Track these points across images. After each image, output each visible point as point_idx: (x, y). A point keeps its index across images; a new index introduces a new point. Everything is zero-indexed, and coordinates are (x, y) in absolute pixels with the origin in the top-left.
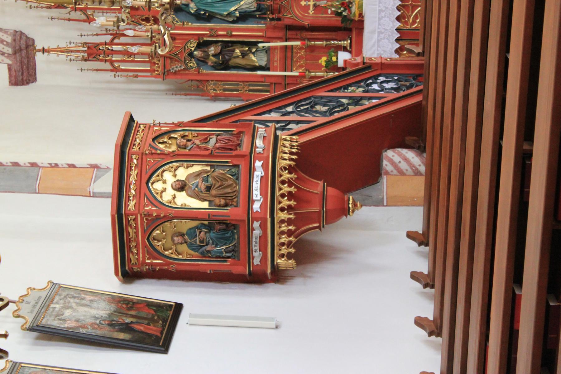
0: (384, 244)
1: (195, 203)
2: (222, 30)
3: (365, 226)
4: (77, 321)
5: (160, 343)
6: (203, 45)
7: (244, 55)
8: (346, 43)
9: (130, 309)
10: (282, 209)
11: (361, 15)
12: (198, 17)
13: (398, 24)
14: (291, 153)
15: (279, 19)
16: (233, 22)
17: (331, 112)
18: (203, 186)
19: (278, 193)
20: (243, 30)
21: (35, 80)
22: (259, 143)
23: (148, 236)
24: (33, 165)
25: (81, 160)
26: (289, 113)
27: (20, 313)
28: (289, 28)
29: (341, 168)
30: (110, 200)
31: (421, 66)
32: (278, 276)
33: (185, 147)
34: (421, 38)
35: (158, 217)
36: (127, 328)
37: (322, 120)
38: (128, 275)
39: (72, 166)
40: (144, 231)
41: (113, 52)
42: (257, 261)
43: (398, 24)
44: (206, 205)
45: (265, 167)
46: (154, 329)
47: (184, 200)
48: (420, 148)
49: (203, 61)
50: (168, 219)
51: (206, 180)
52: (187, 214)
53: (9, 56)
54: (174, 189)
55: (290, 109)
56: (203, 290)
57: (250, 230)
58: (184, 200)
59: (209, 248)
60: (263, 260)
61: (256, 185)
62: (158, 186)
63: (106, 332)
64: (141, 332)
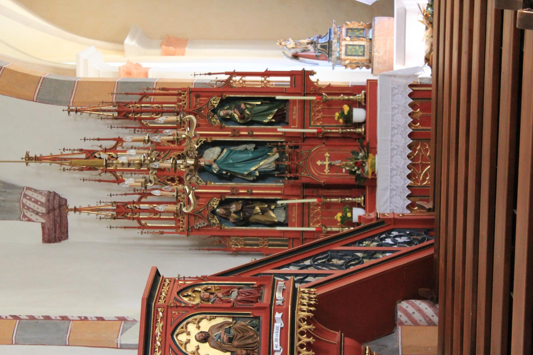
2: (243, 189)
6: (225, 203)
7: (264, 211)
8: (360, 200)
11: (374, 173)
12: (220, 177)
13: (409, 182)
14: (310, 305)
18: (225, 337)
19: (297, 344)
20: (262, 189)
21: (67, 237)
22: (279, 295)
26: (307, 267)
28: (306, 186)
31: (431, 221)
37: (338, 273)
39: (101, 319)
43: (409, 182)
45: (284, 318)
48: (433, 300)
49: (224, 218)
51: (228, 331)
55: (308, 263)
61: (276, 336)
62: (183, 338)
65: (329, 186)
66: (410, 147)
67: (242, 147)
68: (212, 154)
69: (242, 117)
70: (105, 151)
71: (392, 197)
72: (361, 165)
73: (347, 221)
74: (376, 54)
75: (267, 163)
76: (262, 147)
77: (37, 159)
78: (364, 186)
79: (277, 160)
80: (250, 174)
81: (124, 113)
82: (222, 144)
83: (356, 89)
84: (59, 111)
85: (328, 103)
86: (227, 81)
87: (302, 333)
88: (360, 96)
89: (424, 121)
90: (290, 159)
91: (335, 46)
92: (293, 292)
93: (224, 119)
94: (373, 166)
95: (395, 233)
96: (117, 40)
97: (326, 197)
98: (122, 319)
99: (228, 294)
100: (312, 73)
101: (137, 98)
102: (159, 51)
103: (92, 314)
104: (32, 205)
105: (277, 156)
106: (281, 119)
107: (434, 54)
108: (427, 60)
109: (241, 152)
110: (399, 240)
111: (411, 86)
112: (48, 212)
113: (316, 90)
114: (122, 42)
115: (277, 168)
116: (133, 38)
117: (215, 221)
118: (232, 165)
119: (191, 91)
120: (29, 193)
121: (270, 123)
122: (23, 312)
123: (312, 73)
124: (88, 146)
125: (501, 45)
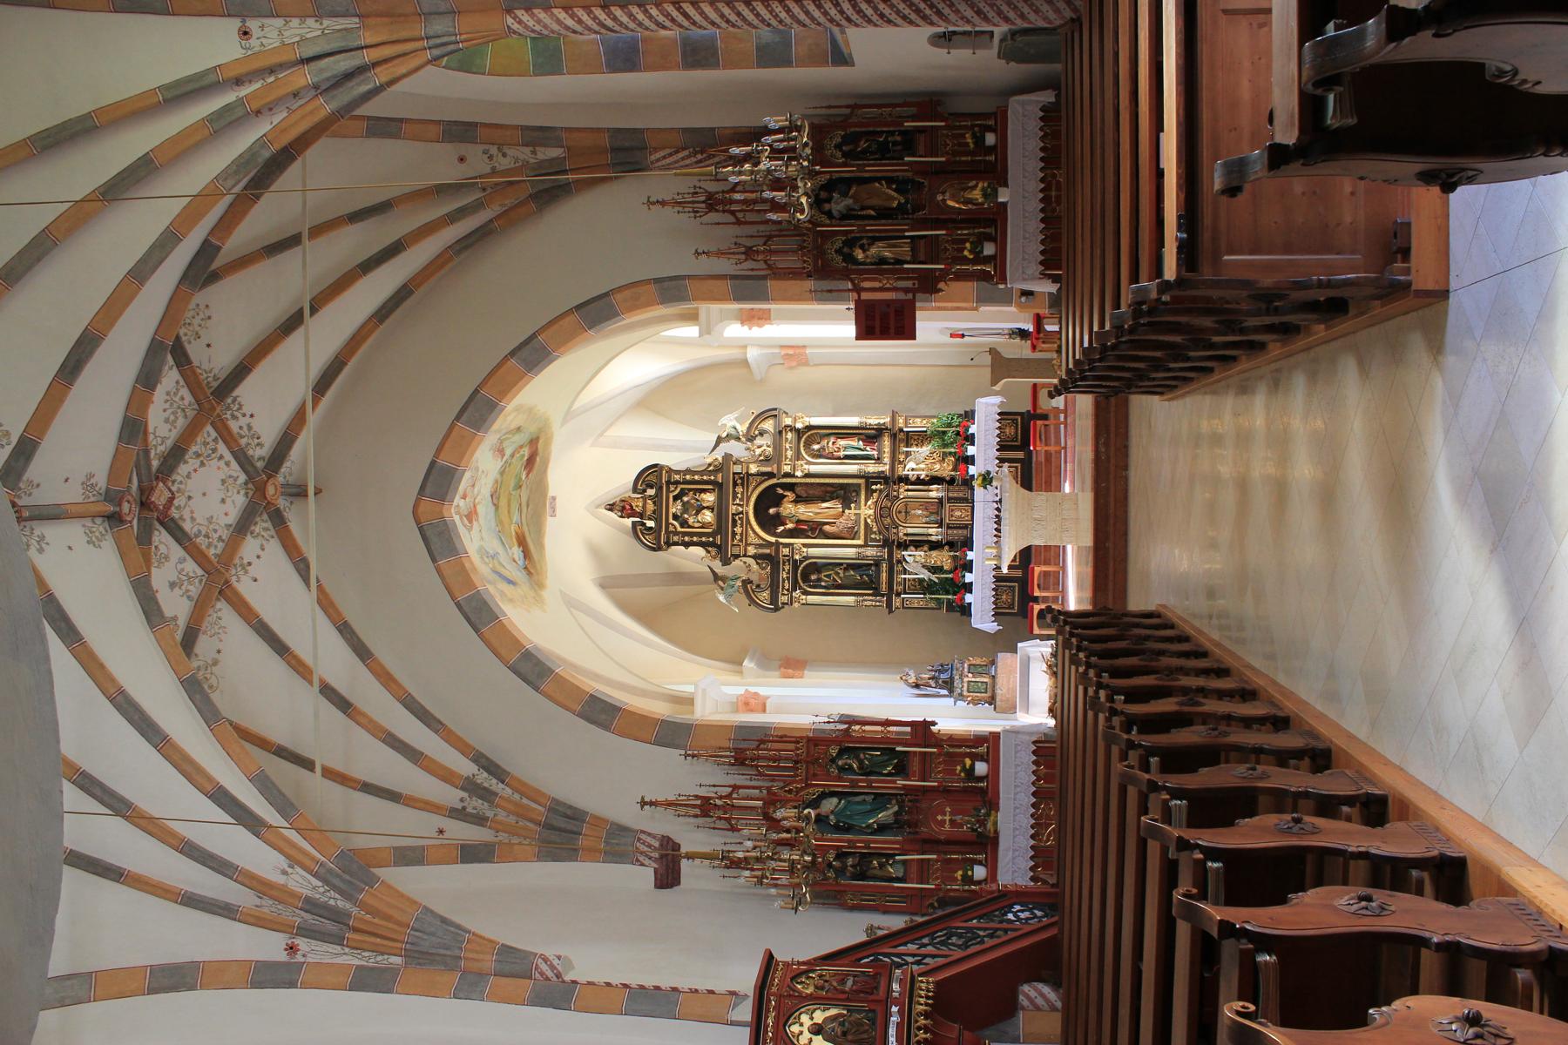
2: (860, 842)
6: (841, 855)
7: (881, 866)
8: (981, 857)
11: (996, 832)
12: (837, 828)
17: (966, 946)
18: (839, 1030)
20: (880, 842)
22: (896, 986)
24: (675, 989)
26: (925, 945)
28: (925, 841)
30: (748, 1030)
31: (1056, 894)
33: (822, 988)
37: (959, 954)
39: (711, 992)
41: (732, 202)
45: (901, 1012)
48: (1056, 984)
49: (840, 872)
51: (842, 1024)
53: (656, 860)
55: (925, 941)
61: (892, 1031)
62: (795, 1028)
65: (948, 842)
66: (1033, 805)
68: (829, 805)
69: (861, 766)
70: (721, 798)
71: (1014, 865)
72: (983, 823)
73: (968, 880)
74: (998, 692)
76: (881, 800)
77: (651, 804)
78: (986, 844)
79: (896, 814)
81: (740, 759)
83: (979, 740)
84: (676, 753)
87: (919, 1029)
88: (982, 750)
91: (957, 682)
92: (914, 979)
93: (842, 769)
94: (995, 823)
97: (946, 853)
98: (733, 993)
100: (934, 724)
102: (777, 673)
103: (702, 986)
105: (896, 808)
106: (901, 770)
107: (1058, 705)
108: (1051, 710)
109: (858, 803)
110: (1022, 915)
111: (1034, 742)
112: (662, 857)
114: (741, 664)
115: (896, 821)
116: (751, 660)
117: (831, 874)
118: (850, 817)
119: (809, 740)
120: (643, 837)
122: (634, 981)
123: (934, 724)
124: (703, 792)
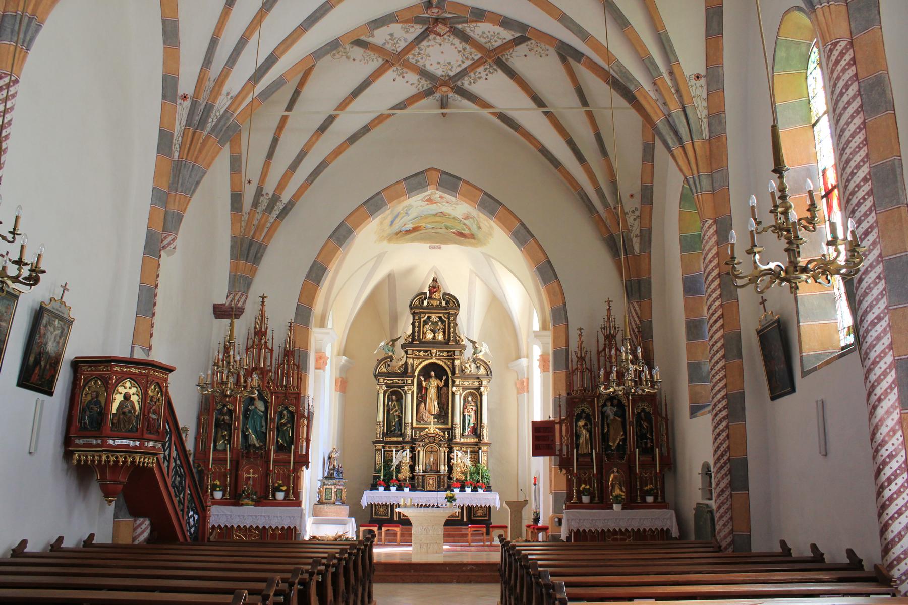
0: (92, 521)
1: (115, 405)
2: (238, 424)
3: (102, 509)
4: (45, 334)
5: (25, 381)
6: (230, 413)
8: (227, 496)
9: (51, 365)
10: (108, 457)
11: (242, 505)
12: (246, 410)
13: (235, 526)
14: (144, 463)
15: (243, 456)
16: (243, 431)
18: (126, 410)
19: (118, 455)
20: (238, 435)
21: (216, 317)
22: (151, 444)
23: (99, 377)
24: (154, 314)
25: (155, 341)
26: (175, 462)
27: (53, 301)
28: (237, 463)
29: (135, 491)
32: (68, 455)
33: (151, 400)
34: (617, 517)
35: (108, 383)
36: (37, 362)
37: (169, 482)
38: (77, 365)
39: (151, 336)
40: (100, 375)
42: (77, 441)
43: (235, 526)
44: (114, 411)
45: (135, 447)
46: (35, 378)
47: (118, 399)
48: (149, 541)
49: (221, 412)
50: (106, 390)
51: (130, 412)
52: (109, 401)
54: (126, 392)
55: (178, 462)
56: (63, 407)
57: (96, 438)
58: (118, 399)
59: (88, 413)
60: (78, 445)
61: (124, 442)
62: (128, 384)
63: (35, 350)
64: (34, 371)
66: (257, 527)
67: (264, 423)
68: (260, 406)
70: (266, 343)
71: (222, 516)
72: (247, 497)
73: (214, 488)
74: (326, 506)
75: (253, 438)
76: (262, 436)
77: (263, 302)
78: (235, 499)
79: (254, 445)
80: (247, 429)
82: (266, 412)
83: (297, 495)
84: (291, 316)
85: (289, 476)
86: (304, 416)
87: (125, 458)
88: (291, 496)
89: (273, 536)
90: (255, 453)
91: (331, 481)
93: (281, 413)
94: (247, 504)
95: (196, 517)
96: (345, 352)
98: (150, 348)
99: (155, 413)
100: (307, 468)
101: (296, 362)
104: (236, 299)
105: (257, 445)
106: (280, 448)
107: (317, 542)
108: (314, 538)
110: (191, 520)
111: (295, 528)
113: (297, 469)
114: (344, 355)
115: (250, 445)
116: (346, 361)
118: (253, 418)
119: (299, 394)
120: (244, 297)
121: (278, 441)
122: (159, 290)
124: (269, 332)
125: (161, 592)
